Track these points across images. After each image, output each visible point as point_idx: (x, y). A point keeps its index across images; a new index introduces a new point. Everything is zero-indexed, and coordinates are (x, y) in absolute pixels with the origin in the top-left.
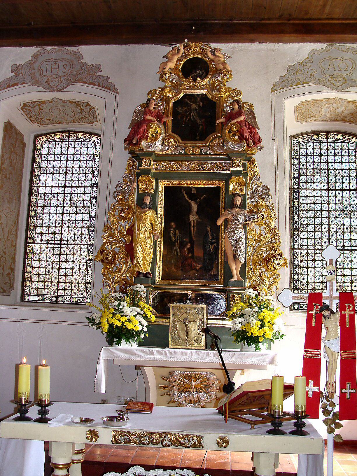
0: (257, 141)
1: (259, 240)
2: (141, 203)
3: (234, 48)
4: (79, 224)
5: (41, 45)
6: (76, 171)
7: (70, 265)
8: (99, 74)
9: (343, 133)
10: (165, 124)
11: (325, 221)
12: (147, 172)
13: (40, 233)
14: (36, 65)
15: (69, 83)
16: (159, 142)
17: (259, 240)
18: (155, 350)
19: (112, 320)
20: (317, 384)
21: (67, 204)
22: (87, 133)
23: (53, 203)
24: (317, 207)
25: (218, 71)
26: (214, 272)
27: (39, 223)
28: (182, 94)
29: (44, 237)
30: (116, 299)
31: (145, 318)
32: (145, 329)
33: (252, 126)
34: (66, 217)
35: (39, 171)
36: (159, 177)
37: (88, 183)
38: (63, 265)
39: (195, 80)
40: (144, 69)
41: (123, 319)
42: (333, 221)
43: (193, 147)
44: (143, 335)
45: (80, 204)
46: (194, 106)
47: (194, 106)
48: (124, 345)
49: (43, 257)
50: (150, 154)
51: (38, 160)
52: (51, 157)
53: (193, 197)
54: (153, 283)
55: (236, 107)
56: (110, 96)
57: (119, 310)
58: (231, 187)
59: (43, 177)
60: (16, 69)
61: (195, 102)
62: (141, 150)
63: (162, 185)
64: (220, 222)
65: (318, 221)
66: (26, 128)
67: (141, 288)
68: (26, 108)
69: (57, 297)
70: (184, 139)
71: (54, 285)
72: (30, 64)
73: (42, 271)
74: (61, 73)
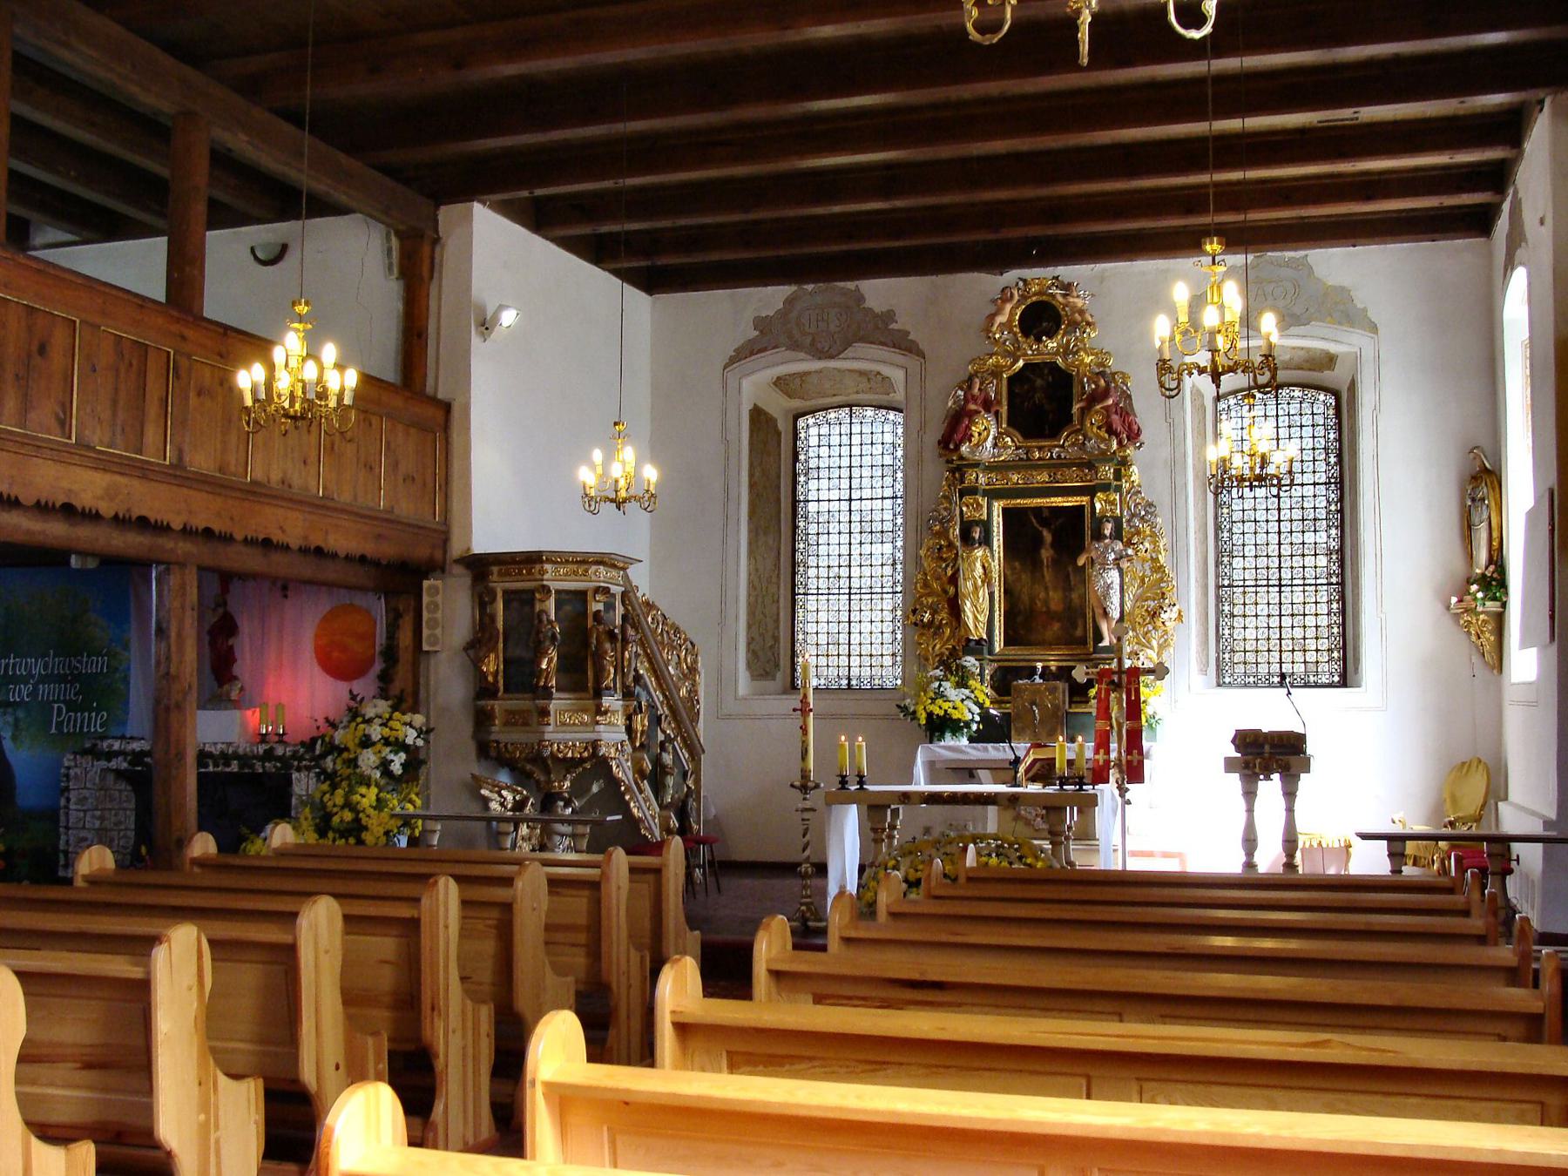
0: (1134, 435)
1: (1143, 581)
2: (966, 537)
3: (1104, 270)
4: (877, 561)
5: (796, 283)
6: (866, 472)
7: (866, 627)
8: (893, 326)
9: (1304, 386)
10: (997, 414)
11: (1274, 538)
12: (973, 491)
13: (813, 576)
14: (794, 314)
15: (847, 344)
16: (988, 438)
17: (1143, 581)
18: (990, 746)
19: (931, 708)
20: (1108, 752)
21: (856, 527)
22: (880, 407)
23: (834, 528)
24: (1261, 515)
25: (1074, 325)
26: (1079, 632)
27: (812, 561)
28: (1021, 363)
29: (823, 584)
30: (937, 679)
31: (977, 703)
32: (977, 718)
33: (1126, 413)
34: (856, 550)
35: (806, 474)
36: (993, 495)
37: (888, 493)
38: (855, 628)
39: (1039, 340)
40: (965, 313)
41: (946, 706)
42: (1285, 539)
43: (1040, 449)
44: (974, 727)
45: (877, 527)
46: (1039, 382)
47: (1039, 382)
48: (949, 740)
49: (823, 616)
50: (976, 465)
51: (802, 457)
52: (824, 451)
53: (1045, 523)
54: (991, 652)
55: (1102, 382)
56: (913, 362)
57: (940, 695)
58: (1098, 506)
59: (813, 485)
60: (761, 324)
61: (1041, 376)
62: (961, 458)
63: (998, 506)
64: (1081, 562)
65: (1261, 538)
66: (777, 406)
67: (970, 661)
68: (780, 383)
69: (849, 679)
70: (1027, 435)
71: (844, 661)
72: (783, 314)
73: (823, 639)
74: (832, 327)
